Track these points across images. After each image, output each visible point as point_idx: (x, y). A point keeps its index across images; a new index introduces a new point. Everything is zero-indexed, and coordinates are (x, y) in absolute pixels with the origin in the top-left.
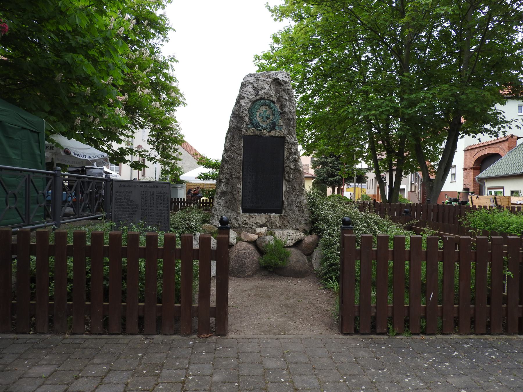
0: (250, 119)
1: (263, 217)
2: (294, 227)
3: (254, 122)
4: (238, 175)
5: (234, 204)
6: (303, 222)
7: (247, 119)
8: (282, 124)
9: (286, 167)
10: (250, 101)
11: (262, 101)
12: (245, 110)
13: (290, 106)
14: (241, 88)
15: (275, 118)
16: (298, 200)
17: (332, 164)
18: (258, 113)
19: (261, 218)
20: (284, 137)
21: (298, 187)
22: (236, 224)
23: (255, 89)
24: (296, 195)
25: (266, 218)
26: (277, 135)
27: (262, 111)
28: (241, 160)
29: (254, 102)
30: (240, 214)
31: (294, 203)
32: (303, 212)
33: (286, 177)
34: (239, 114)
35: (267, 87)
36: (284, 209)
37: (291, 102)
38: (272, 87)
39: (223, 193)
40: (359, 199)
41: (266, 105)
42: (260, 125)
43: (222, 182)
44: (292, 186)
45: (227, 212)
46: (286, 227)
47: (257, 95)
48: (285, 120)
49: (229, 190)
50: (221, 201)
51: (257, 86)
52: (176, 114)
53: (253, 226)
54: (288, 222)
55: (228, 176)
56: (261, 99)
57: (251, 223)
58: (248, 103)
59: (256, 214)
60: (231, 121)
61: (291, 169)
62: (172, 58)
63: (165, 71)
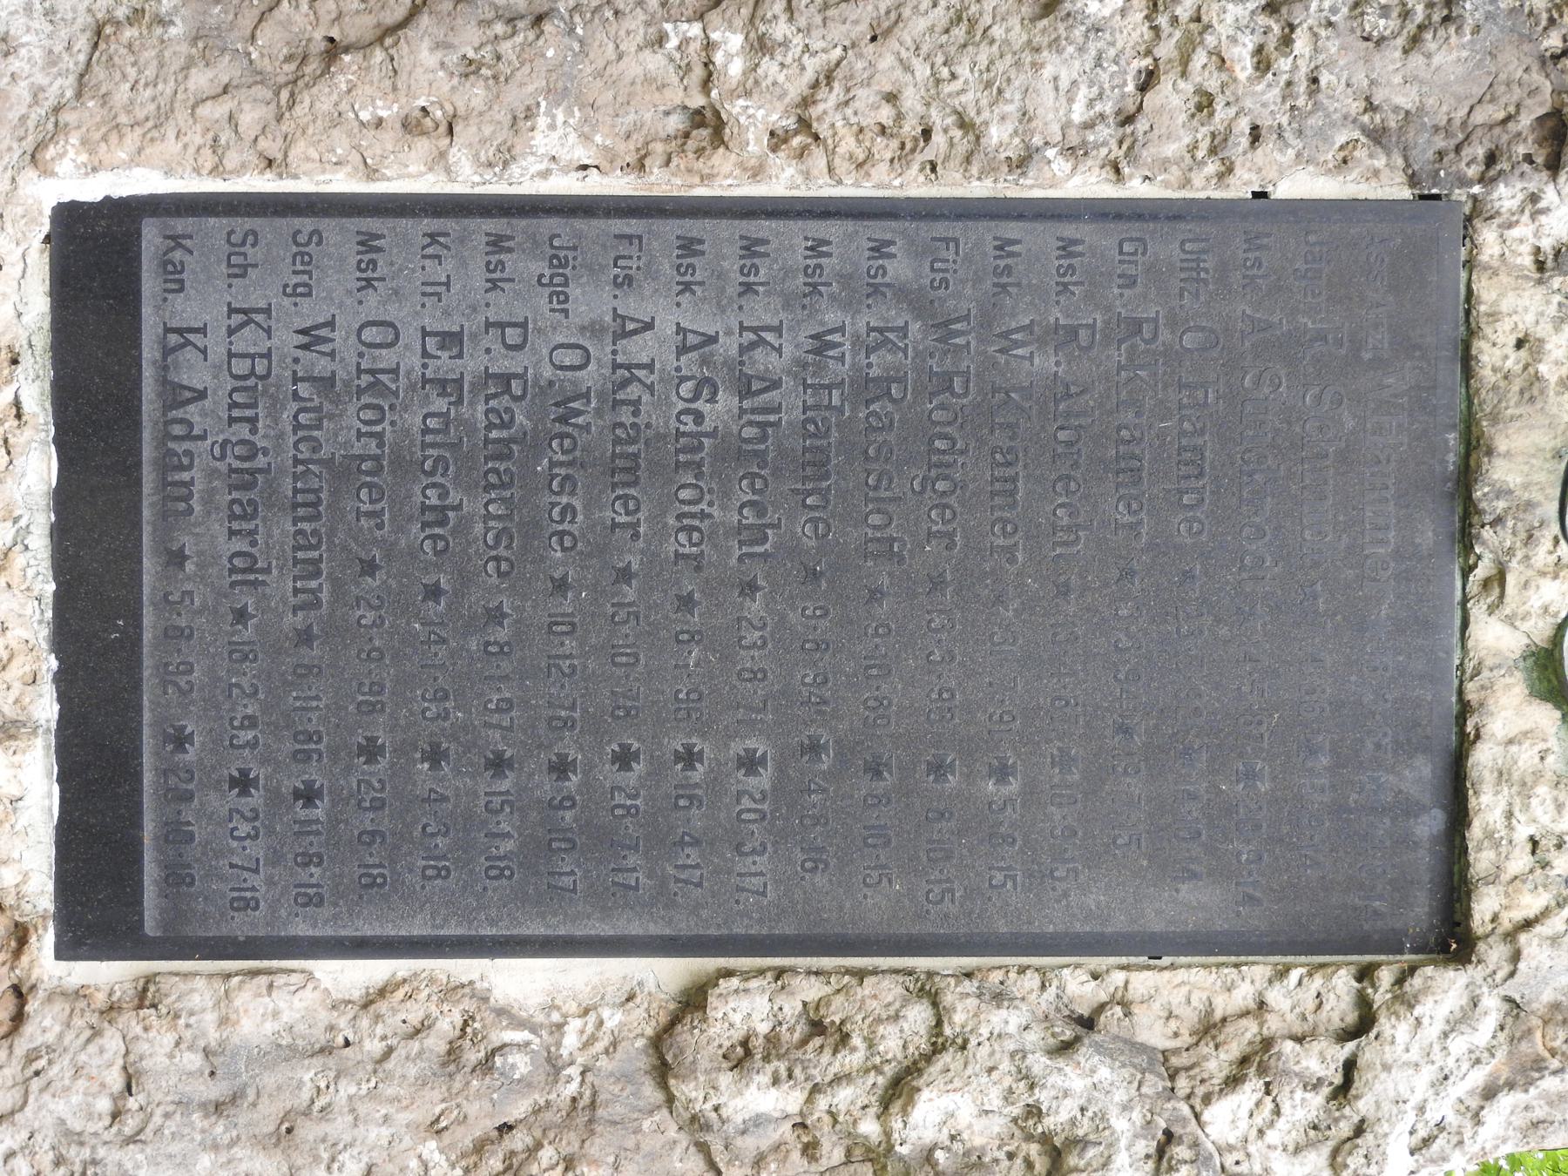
4: (754, 119)
20: (1453, 940)
26: (1488, 807)
36: (145, 996)
61: (899, 1089)
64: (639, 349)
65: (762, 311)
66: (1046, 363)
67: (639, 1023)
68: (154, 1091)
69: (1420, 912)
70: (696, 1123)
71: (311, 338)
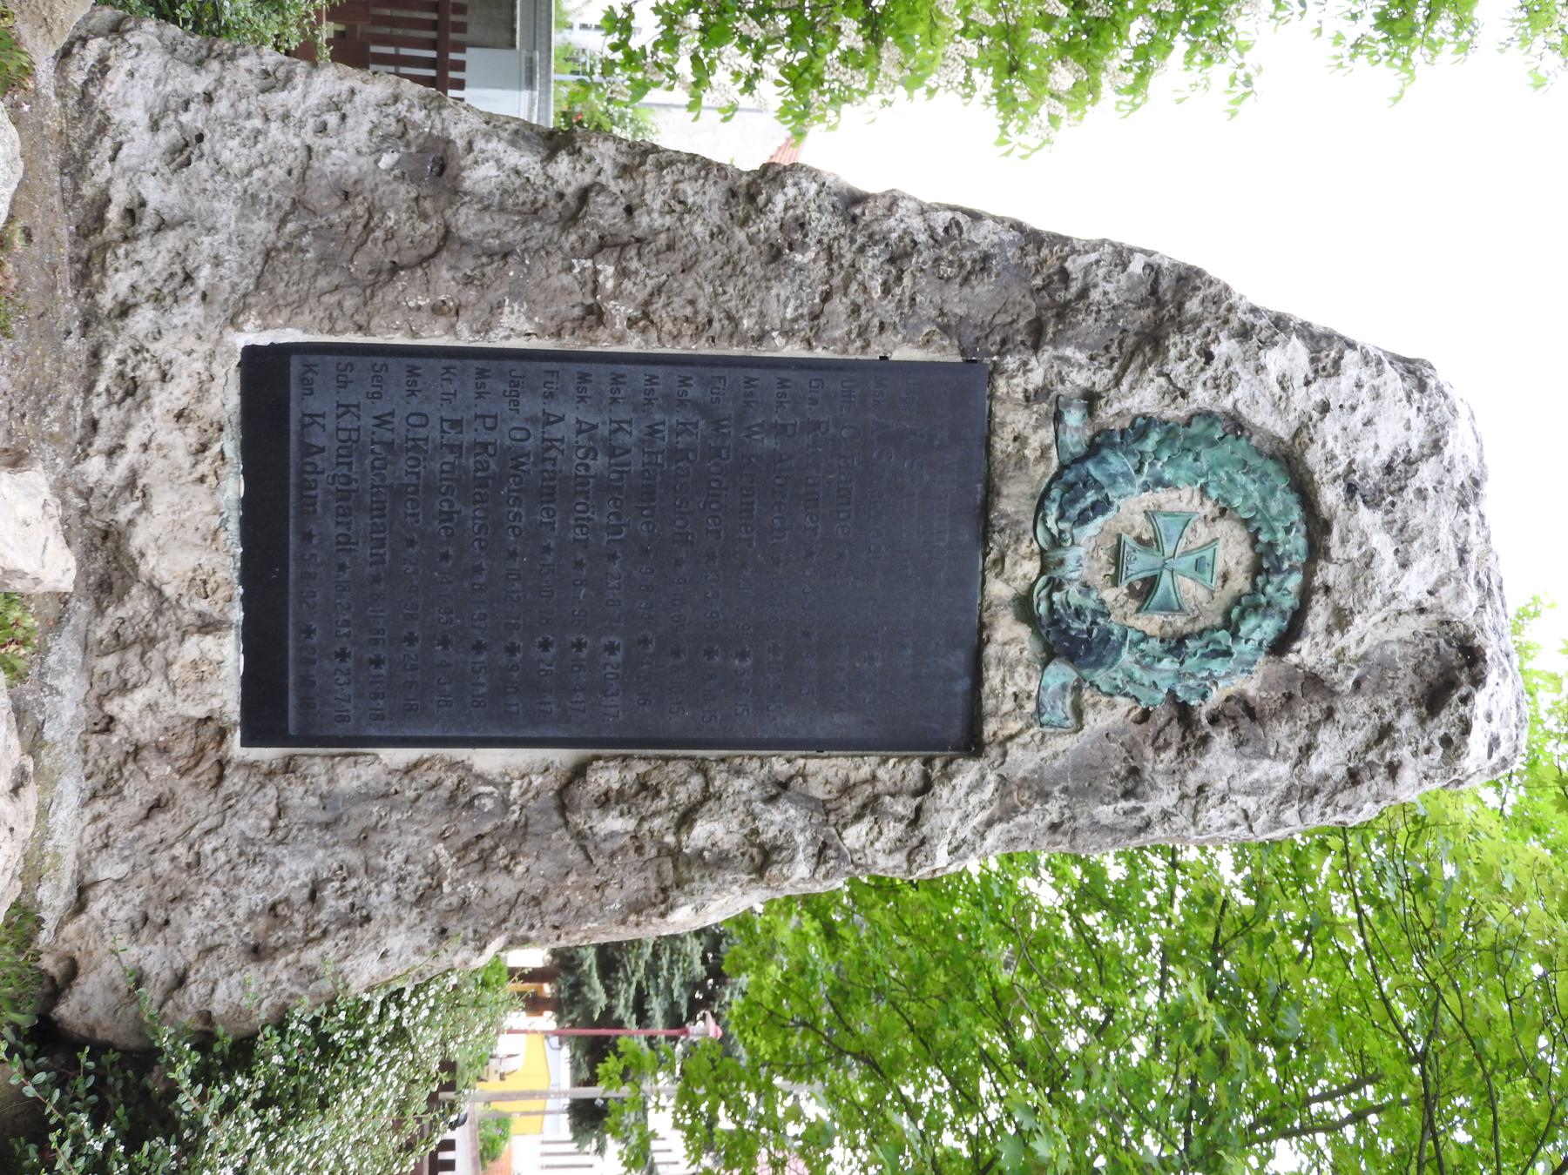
0: (1142, 426)
1: (209, 560)
2: (108, 869)
3: (1117, 462)
4: (619, 311)
5: (326, 262)
6: (154, 958)
7: (1142, 397)
8: (1100, 720)
9: (702, 769)
10: (1303, 430)
11: (1295, 544)
13: (1254, 790)
14: (1396, 359)
16: (382, 900)
17: (671, 962)
18: (1184, 499)
19: (191, 531)
20: (973, 745)
21: (504, 886)
22: (118, 283)
23: (1398, 470)
24: (435, 871)
25: (201, 585)
26: (993, 677)
27: (1203, 534)
28: (761, 338)
29: (1289, 463)
30: (233, 322)
31: (353, 857)
32: (257, 953)
33: (607, 777)
34: (1180, 324)
35: (1414, 586)
36: (288, 767)
37: (1286, 798)
38: (1411, 625)
39: (437, 167)
41: (1257, 570)
42: (1083, 519)
43: (551, 157)
44: (522, 830)
45: (250, 201)
46: (105, 787)
47: (1351, 489)
48: (1131, 749)
49: (467, 222)
50: (358, 133)
51: (1421, 493)
52: (948, 100)
53: (111, 453)
54: (157, 806)
55: (604, 213)
56: (1318, 527)
57: (134, 439)
58: (1279, 406)
59: (234, 487)
60: (1122, 256)
61: (686, 819)
62: (1248, 82)
63: (1181, 44)
64: (557, 431)
65: (622, 412)
66: (770, 443)
67: (551, 782)
68: (295, 816)
69: (956, 730)
70: (580, 836)
71: (382, 421)
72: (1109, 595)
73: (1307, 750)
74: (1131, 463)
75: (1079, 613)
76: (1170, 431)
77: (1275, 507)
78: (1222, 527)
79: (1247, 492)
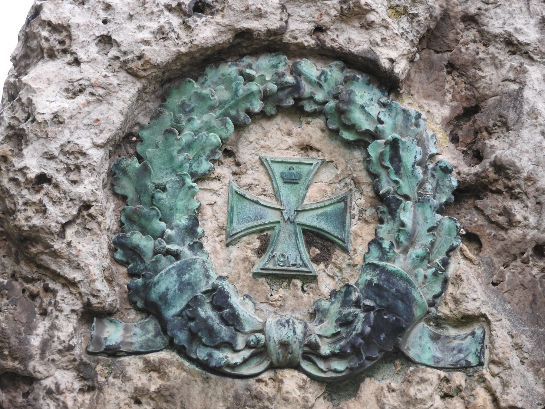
0: (124, 252)
3: (166, 282)
7: (90, 254)
8: (475, 294)
10: (129, 66)
11: (264, 69)
12: (74, 160)
15: (406, 239)
18: (212, 201)
27: (254, 175)
40: (473, 334)
41: (297, 111)
42: (233, 320)
48: (512, 254)
56: (244, 44)
58: (100, 94)
72: (326, 285)
73: (513, 46)
74: (167, 265)
75: (345, 322)
76: (131, 220)
77: (222, 94)
78: (246, 153)
79: (204, 127)
